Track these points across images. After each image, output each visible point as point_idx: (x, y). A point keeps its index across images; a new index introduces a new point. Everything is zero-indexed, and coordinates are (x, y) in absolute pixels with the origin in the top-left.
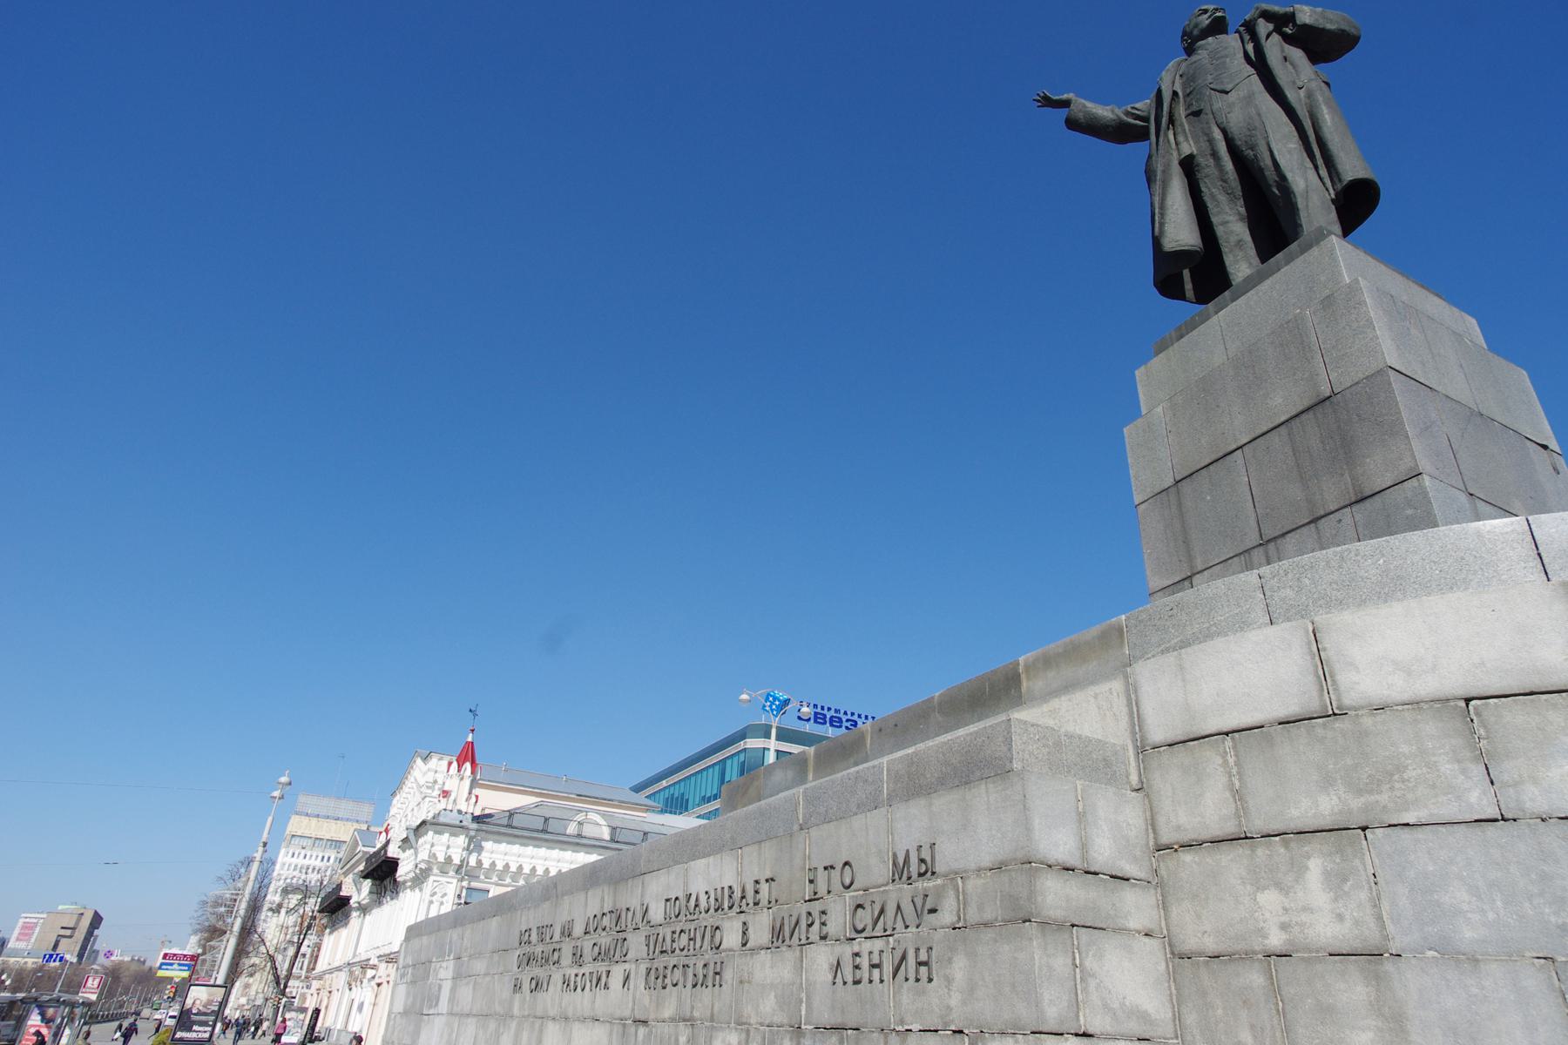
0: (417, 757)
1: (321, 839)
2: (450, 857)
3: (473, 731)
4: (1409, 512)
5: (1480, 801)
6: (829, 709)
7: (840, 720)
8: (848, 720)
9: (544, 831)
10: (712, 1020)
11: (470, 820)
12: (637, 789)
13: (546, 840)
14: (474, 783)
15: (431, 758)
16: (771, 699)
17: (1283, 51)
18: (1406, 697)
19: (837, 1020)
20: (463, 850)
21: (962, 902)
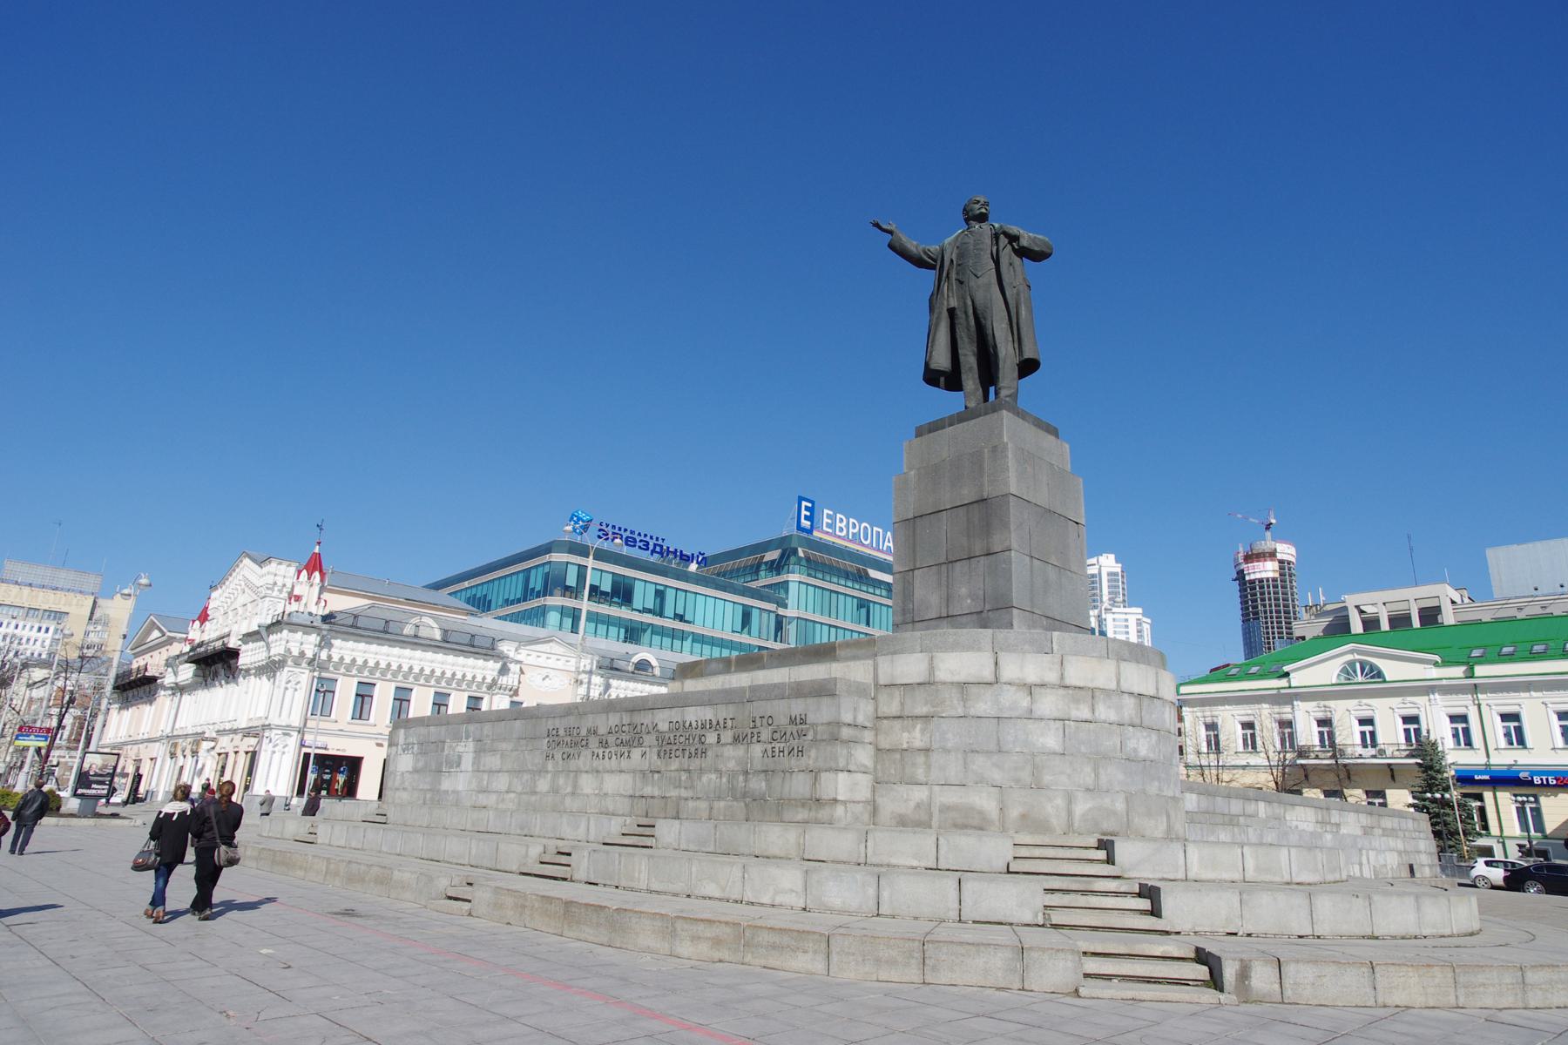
0: (245, 557)
1: (35, 609)
2: (303, 651)
3: (319, 543)
4: (1004, 566)
5: (960, 712)
6: (626, 530)
7: (635, 541)
8: (641, 541)
9: (386, 632)
10: (701, 770)
11: (320, 621)
12: (437, 586)
13: (388, 640)
14: (322, 589)
15: (270, 562)
16: (575, 519)
17: (1010, 258)
18: (951, 681)
19: (764, 768)
20: (316, 646)
21: (815, 734)
